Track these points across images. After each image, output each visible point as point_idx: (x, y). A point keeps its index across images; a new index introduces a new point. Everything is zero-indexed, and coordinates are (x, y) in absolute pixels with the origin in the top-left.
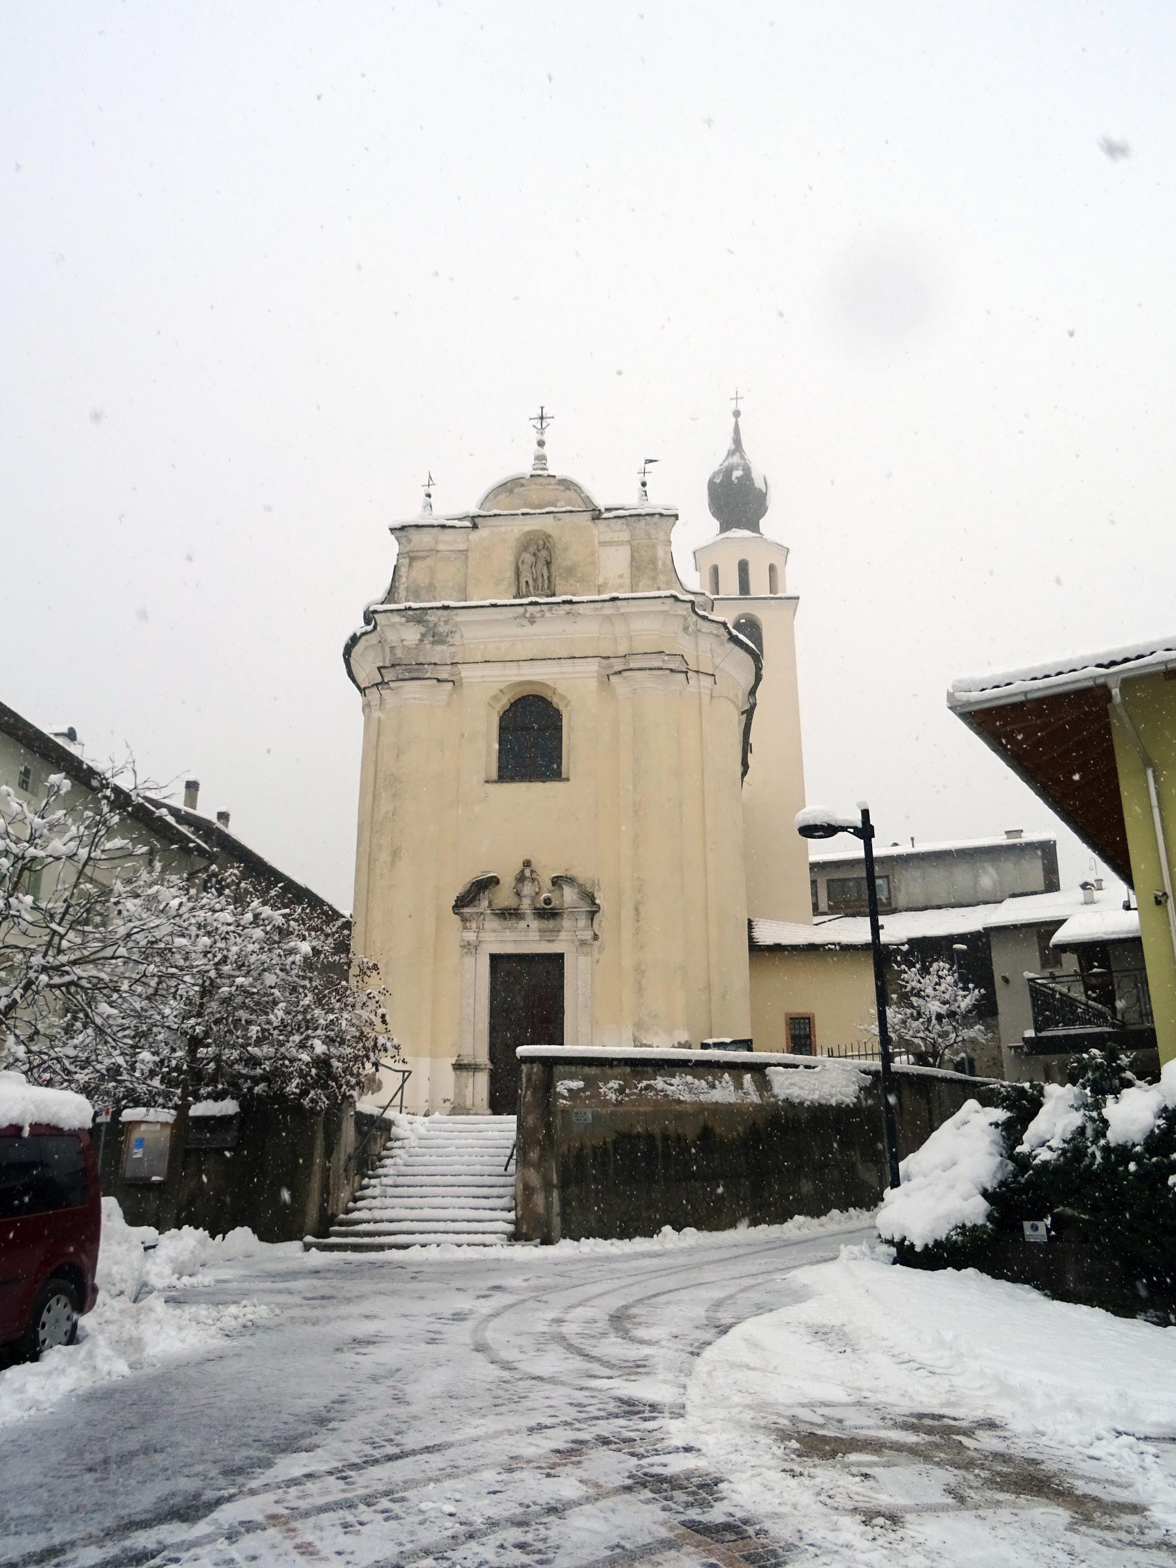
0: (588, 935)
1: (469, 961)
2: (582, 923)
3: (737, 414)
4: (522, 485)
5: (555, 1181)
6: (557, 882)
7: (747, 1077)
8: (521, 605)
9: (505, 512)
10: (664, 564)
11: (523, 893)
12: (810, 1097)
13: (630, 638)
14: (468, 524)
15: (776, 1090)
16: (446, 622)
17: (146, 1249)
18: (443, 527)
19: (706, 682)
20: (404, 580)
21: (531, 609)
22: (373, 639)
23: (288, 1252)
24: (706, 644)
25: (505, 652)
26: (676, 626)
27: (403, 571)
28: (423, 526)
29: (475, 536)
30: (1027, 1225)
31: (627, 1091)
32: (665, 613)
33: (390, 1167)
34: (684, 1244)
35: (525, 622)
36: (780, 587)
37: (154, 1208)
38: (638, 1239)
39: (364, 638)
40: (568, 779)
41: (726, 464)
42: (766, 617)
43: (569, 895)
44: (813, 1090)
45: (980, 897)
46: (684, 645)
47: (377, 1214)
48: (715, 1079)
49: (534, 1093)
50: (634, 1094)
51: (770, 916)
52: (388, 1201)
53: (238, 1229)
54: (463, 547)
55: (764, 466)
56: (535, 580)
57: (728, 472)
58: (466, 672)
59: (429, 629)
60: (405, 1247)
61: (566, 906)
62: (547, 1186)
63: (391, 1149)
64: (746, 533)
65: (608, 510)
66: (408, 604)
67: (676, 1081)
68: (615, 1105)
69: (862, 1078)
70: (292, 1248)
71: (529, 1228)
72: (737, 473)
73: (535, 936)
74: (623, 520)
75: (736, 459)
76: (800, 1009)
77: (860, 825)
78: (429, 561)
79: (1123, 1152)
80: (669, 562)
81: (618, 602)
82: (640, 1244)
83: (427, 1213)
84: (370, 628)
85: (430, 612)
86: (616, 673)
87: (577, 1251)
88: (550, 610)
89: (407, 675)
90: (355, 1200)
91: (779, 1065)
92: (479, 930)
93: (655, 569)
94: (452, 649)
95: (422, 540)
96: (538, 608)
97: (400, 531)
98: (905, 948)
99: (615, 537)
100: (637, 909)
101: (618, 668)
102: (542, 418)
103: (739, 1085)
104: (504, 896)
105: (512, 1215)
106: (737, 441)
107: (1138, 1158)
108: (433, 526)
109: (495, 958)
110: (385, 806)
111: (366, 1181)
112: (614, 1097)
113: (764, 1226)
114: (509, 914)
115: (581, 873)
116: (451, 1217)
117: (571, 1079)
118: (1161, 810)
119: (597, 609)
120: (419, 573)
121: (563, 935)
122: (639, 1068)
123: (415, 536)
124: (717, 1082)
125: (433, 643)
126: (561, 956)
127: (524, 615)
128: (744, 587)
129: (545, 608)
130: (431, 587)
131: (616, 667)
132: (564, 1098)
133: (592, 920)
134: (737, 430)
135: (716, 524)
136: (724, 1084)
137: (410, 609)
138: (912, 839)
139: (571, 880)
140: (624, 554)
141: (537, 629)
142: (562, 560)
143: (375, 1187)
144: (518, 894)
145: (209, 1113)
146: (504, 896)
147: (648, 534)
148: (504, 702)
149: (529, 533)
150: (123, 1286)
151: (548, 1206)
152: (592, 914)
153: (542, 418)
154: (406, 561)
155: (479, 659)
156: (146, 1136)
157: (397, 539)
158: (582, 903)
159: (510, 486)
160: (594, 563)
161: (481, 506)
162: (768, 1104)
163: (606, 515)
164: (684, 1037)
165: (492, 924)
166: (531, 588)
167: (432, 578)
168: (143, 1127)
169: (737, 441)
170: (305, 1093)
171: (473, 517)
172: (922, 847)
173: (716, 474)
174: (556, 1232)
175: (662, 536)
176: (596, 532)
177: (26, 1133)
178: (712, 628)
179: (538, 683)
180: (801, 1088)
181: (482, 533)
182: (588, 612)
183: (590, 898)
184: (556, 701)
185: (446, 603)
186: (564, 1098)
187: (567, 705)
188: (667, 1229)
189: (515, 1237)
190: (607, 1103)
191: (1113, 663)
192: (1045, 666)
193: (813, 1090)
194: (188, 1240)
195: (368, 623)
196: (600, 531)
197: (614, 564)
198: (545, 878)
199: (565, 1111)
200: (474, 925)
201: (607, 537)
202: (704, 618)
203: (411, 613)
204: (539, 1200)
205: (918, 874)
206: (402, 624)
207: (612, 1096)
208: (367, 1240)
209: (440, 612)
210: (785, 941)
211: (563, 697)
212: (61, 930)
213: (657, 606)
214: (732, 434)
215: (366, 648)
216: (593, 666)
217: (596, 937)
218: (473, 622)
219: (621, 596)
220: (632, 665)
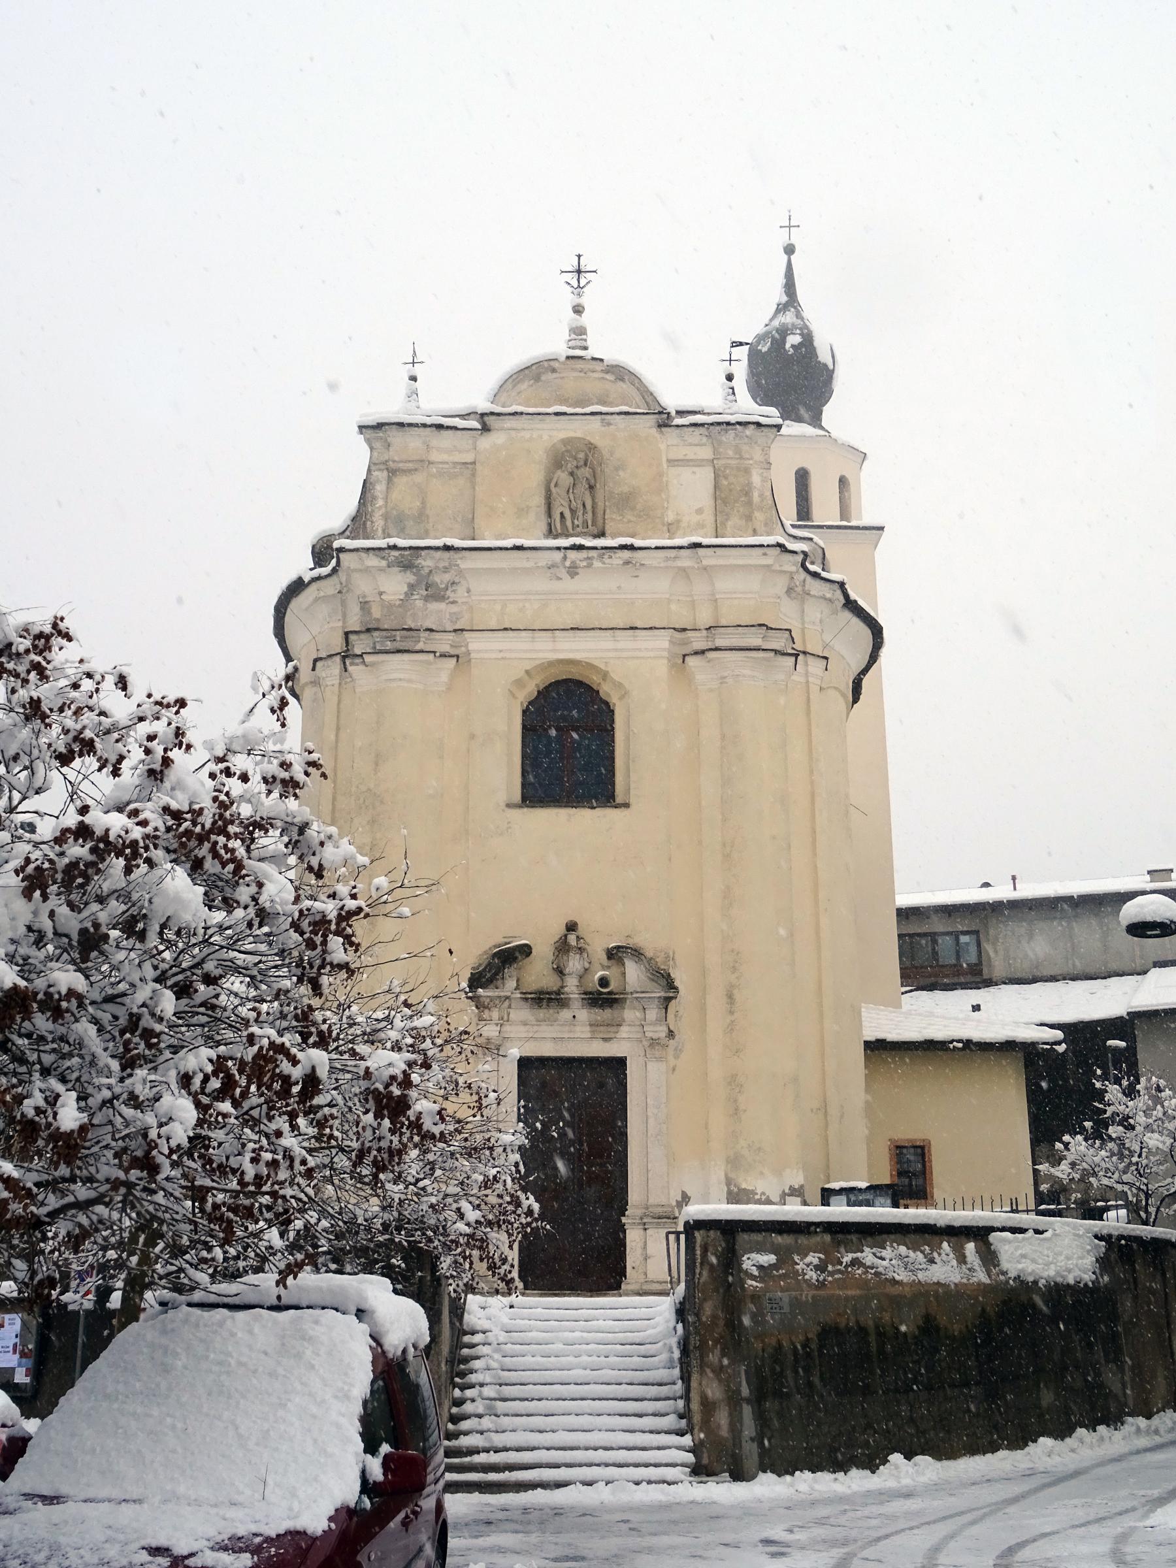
2: (653, 1014)
3: (790, 250)
4: (554, 370)
5: (745, 1391)
6: (615, 955)
7: (970, 1247)
8: (559, 548)
9: (531, 410)
10: (761, 495)
11: (567, 971)
12: (1045, 1274)
14: (475, 424)
15: (1005, 1265)
16: (446, 570)
18: (440, 427)
19: (816, 666)
20: (380, 502)
21: (572, 555)
22: (329, 588)
24: (815, 612)
25: (538, 611)
27: (380, 489)
28: (410, 425)
29: (486, 442)
31: (830, 1268)
34: (923, 1479)
36: (853, 513)
39: (314, 586)
40: (626, 805)
41: (776, 323)
43: (634, 974)
44: (1048, 1264)
45: (1114, 966)
46: (787, 614)
47: (498, 1440)
48: (932, 1250)
50: (839, 1271)
52: (506, 1421)
54: (469, 458)
58: (476, 644)
61: (629, 989)
62: (734, 1400)
63: (472, 1346)
65: (680, 413)
66: (392, 541)
67: (887, 1253)
68: (817, 1288)
69: (1097, 1246)
72: (794, 339)
73: (583, 1031)
74: (702, 430)
75: (789, 318)
76: (908, 1133)
78: (419, 478)
80: (769, 493)
81: (701, 551)
82: (857, 1481)
85: (423, 553)
86: (696, 653)
87: (792, 1491)
88: (601, 557)
89: (389, 645)
90: (455, 1419)
91: (1003, 1229)
92: (503, 1021)
93: (750, 503)
94: (454, 609)
95: (409, 445)
96: (584, 554)
97: (374, 430)
100: (730, 997)
104: (537, 972)
105: (687, 1440)
108: (424, 425)
112: (815, 1277)
114: (547, 999)
116: (602, 1444)
117: (759, 1251)
119: (667, 559)
120: (403, 495)
121: (624, 1032)
122: (840, 1237)
123: (397, 438)
124: (935, 1255)
125: (426, 599)
128: (804, 511)
130: (421, 516)
131: (695, 645)
132: (753, 1278)
133: (666, 1009)
136: (944, 1257)
138: (1014, 878)
139: (637, 953)
140: (705, 476)
141: (584, 583)
144: (560, 972)
146: (537, 972)
147: (738, 451)
148: (530, 690)
149: (566, 442)
155: (494, 625)
157: (368, 441)
158: (650, 986)
159: (535, 372)
161: (495, 399)
162: (999, 1283)
163: (679, 421)
164: (796, 1179)
165: (521, 1012)
166: (569, 523)
167: (423, 502)
171: (483, 415)
172: (1027, 891)
175: (758, 455)
176: (663, 447)
179: (590, 666)
180: (1034, 1261)
182: (655, 563)
184: (606, 690)
185: (450, 541)
187: (622, 698)
188: (896, 1458)
189: (700, 1471)
193: (1048, 1264)
196: (670, 444)
198: (597, 948)
199: (755, 1297)
200: (495, 1014)
202: (815, 575)
203: (396, 553)
204: (722, 1418)
205: (1023, 931)
206: (381, 570)
207: (812, 1275)
208: (493, 1477)
209: (439, 554)
210: (892, 1036)
211: (619, 685)
213: (755, 558)
214: (781, 280)
215: (317, 600)
216: (662, 642)
217: (671, 1034)
219: (705, 541)
220: (719, 643)
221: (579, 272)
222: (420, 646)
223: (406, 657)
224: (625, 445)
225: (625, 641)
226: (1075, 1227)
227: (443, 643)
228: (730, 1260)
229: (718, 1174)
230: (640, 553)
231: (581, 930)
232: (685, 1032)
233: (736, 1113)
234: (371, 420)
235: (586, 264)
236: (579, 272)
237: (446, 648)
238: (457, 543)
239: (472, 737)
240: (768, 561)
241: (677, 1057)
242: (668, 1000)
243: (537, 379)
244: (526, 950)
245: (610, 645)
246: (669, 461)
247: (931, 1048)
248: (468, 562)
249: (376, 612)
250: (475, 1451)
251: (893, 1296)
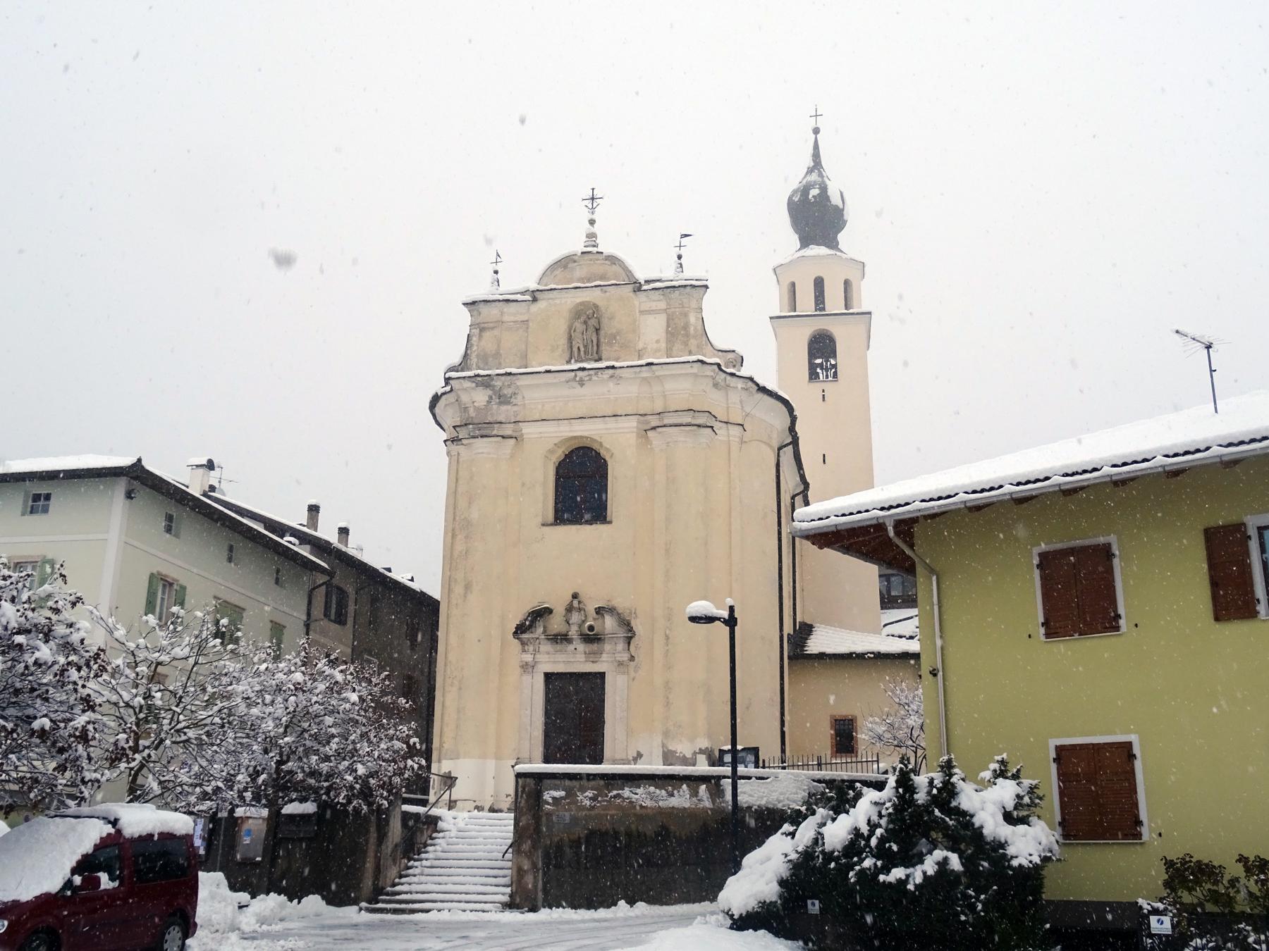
0: (625, 657)
1: (527, 678)
2: (621, 646)
3: (816, 131)
6: (599, 611)
10: (695, 329)
13: (665, 396)
14: (528, 297)
16: (509, 386)
17: (240, 907)
18: (508, 301)
19: (736, 431)
20: (475, 348)
21: (580, 374)
22: (450, 398)
23: (350, 913)
25: (561, 407)
26: (706, 385)
29: (535, 308)
30: (809, 902)
32: (696, 375)
33: (431, 853)
34: (632, 914)
35: (575, 384)
36: (855, 302)
37: (247, 879)
38: (601, 910)
40: (610, 522)
42: (839, 331)
43: (609, 623)
47: (414, 888)
49: (527, 801)
51: (832, 621)
52: (423, 878)
53: (311, 896)
55: (840, 183)
56: (585, 346)
57: (805, 190)
60: (427, 911)
64: (823, 250)
65: (647, 282)
70: (352, 910)
71: (520, 900)
72: (814, 192)
73: (581, 657)
75: (814, 177)
76: (844, 711)
77: (726, 617)
78: (496, 332)
79: (829, 856)
81: (654, 367)
82: (602, 913)
83: (450, 887)
84: (448, 388)
90: (401, 877)
92: (536, 652)
93: (687, 335)
94: (515, 408)
95: (490, 313)
96: (586, 373)
97: (471, 305)
98: (78, 880)
99: (654, 305)
101: (654, 424)
102: (593, 199)
103: (695, 793)
104: (556, 623)
105: (508, 890)
107: (837, 859)
109: (548, 676)
110: (460, 547)
111: (411, 863)
113: (707, 903)
114: (561, 639)
115: (620, 603)
118: (940, 608)
120: (487, 343)
123: (484, 309)
125: (500, 403)
126: (602, 675)
129: (592, 372)
130: (497, 355)
131: (653, 424)
132: (548, 803)
135: (794, 239)
137: (478, 375)
139: (612, 610)
141: (586, 390)
142: (607, 329)
143: (417, 867)
145: (296, 812)
146: (556, 623)
148: (559, 455)
149: (582, 303)
150: (217, 927)
151: (535, 887)
152: (629, 640)
153: (593, 199)
154: (476, 331)
155: (537, 417)
156: (252, 827)
159: (565, 263)
163: (644, 288)
165: (546, 647)
168: (250, 821)
170: (349, 802)
173: (795, 192)
174: (540, 903)
175: (694, 304)
176: (637, 303)
177: (156, 838)
178: (740, 384)
179: (582, 437)
181: (541, 305)
183: (626, 625)
185: (509, 370)
186: (548, 803)
188: (622, 903)
189: (510, 905)
190: (584, 808)
191: (891, 507)
192: (850, 506)
194: (271, 902)
195: (447, 384)
196: (641, 301)
197: (653, 329)
199: (549, 814)
200: (531, 648)
201: (645, 307)
202: (732, 375)
208: (403, 906)
211: (607, 449)
212: (178, 710)
213: (687, 369)
214: (811, 150)
216: (632, 423)
217: (632, 658)
219: (655, 361)
220: (666, 421)
222: (495, 432)
224: (615, 304)
225: (611, 424)
226: (798, 776)
227: (508, 431)
228: (537, 796)
229: (658, 740)
230: (618, 371)
231: (582, 597)
232: (641, 657)
233: (668, 704)
234: (469, 300)
235: (597, 193)
237: (508, 432)
238: (514, 370)
239: (523, 484)
241: (636, 671)
242: (630, 638)
243: (565, 267)
244: (549, 611)
245: (602, 426)
246: (641, 312)
247: (880, 657)
249: (472, 413)
250: (399, 893)
251: (645, 816)
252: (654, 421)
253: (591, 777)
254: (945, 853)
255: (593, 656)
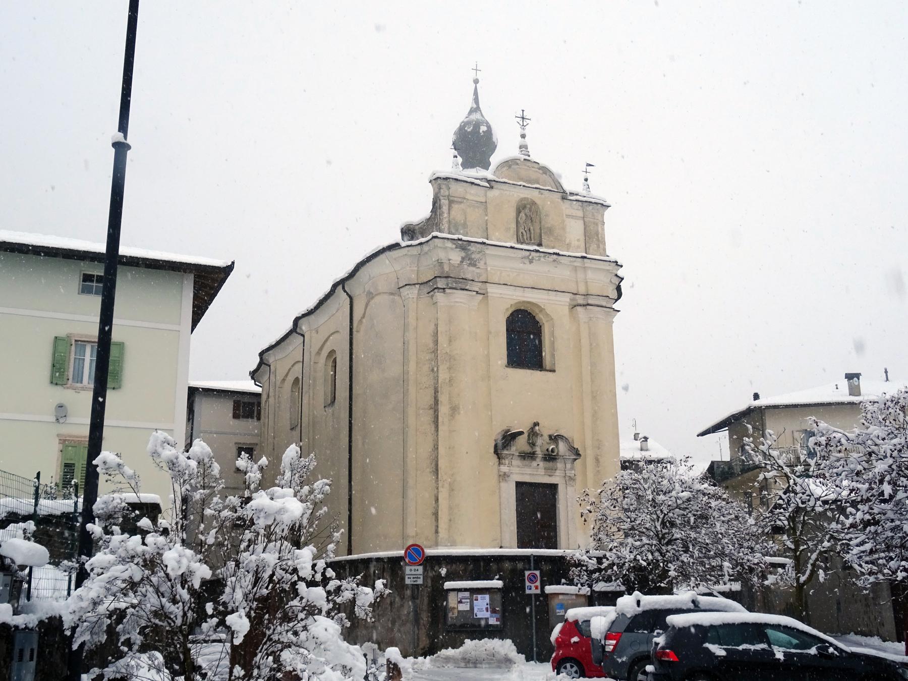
2: (569, 466)
3: (476, 81)
18: (472, 183)
20: (445, 215)
21: (533, 254)
29: (492, 194)
35: (527, 261)
43: (562, 447)
54: (484, 200)
59: (467, 255)
65: (572, 194)
66: (460, 237)
72: (483, 128)
73: (541, 471)
78: (462, 206)
81: (585, 260)
92: (510, 465)
94: (478, 271)
96: (538, 254)
106: (476, 100)
109: (519, 485)
114: (528, 456)
121: (558, 473)
125: (470, 265)
127: (528, 257)
129: (542, 255)
130: (465, 225)
134: (476, 93)
137: (461, 240)
147: (593, 215)
149: (522, 200)
160: (564, 229)
165: (516, 462)
169: (476, 100)
175: (600, 218)
179: (529, 303)
184: (540, 317)
196: (565, 207)
197: (575, 231)
200: (507, 462)
203: (460, 242)
214: (472, 97)
218: (500, 256)
220: (590, 302)
221: (523, 118)
223: (465, 292)
224: (547, 202)
227: (476, 287)
236: (523, 118)
240: (608, 268)
243: (510, 167)
244: (521, 433)
245: (545, 297)
248: (490, 251)
249: (446, 268)
252: (580, 300)
253: (539, 559)
254: (20, 621)
255: (550, 471)
